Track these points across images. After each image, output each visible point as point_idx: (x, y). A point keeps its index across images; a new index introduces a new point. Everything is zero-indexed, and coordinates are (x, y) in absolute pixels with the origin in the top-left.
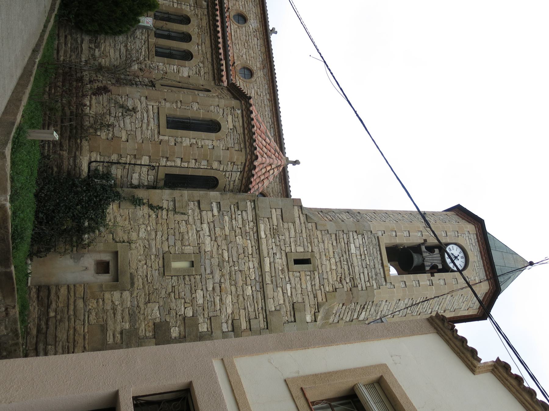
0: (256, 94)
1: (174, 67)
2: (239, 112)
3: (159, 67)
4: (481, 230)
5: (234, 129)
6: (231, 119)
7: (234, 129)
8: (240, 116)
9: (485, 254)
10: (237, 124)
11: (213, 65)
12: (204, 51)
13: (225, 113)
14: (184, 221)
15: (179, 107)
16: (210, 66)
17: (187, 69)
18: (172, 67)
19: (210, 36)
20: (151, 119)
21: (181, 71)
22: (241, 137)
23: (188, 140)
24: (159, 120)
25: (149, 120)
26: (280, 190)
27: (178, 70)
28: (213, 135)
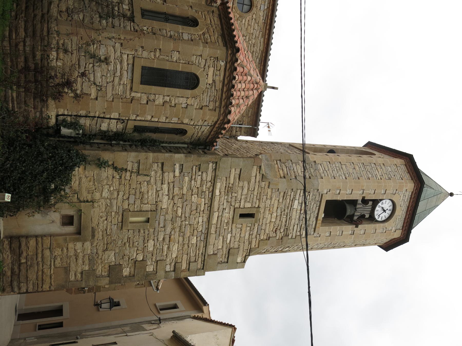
2: (223, 64)
6: (213, 72)
8: (223, 69)
10: (217, 78)
15: (157, 56)
20: (124, 72)
22: (218, 94)
23: (161, 97)
28: (189, 92)
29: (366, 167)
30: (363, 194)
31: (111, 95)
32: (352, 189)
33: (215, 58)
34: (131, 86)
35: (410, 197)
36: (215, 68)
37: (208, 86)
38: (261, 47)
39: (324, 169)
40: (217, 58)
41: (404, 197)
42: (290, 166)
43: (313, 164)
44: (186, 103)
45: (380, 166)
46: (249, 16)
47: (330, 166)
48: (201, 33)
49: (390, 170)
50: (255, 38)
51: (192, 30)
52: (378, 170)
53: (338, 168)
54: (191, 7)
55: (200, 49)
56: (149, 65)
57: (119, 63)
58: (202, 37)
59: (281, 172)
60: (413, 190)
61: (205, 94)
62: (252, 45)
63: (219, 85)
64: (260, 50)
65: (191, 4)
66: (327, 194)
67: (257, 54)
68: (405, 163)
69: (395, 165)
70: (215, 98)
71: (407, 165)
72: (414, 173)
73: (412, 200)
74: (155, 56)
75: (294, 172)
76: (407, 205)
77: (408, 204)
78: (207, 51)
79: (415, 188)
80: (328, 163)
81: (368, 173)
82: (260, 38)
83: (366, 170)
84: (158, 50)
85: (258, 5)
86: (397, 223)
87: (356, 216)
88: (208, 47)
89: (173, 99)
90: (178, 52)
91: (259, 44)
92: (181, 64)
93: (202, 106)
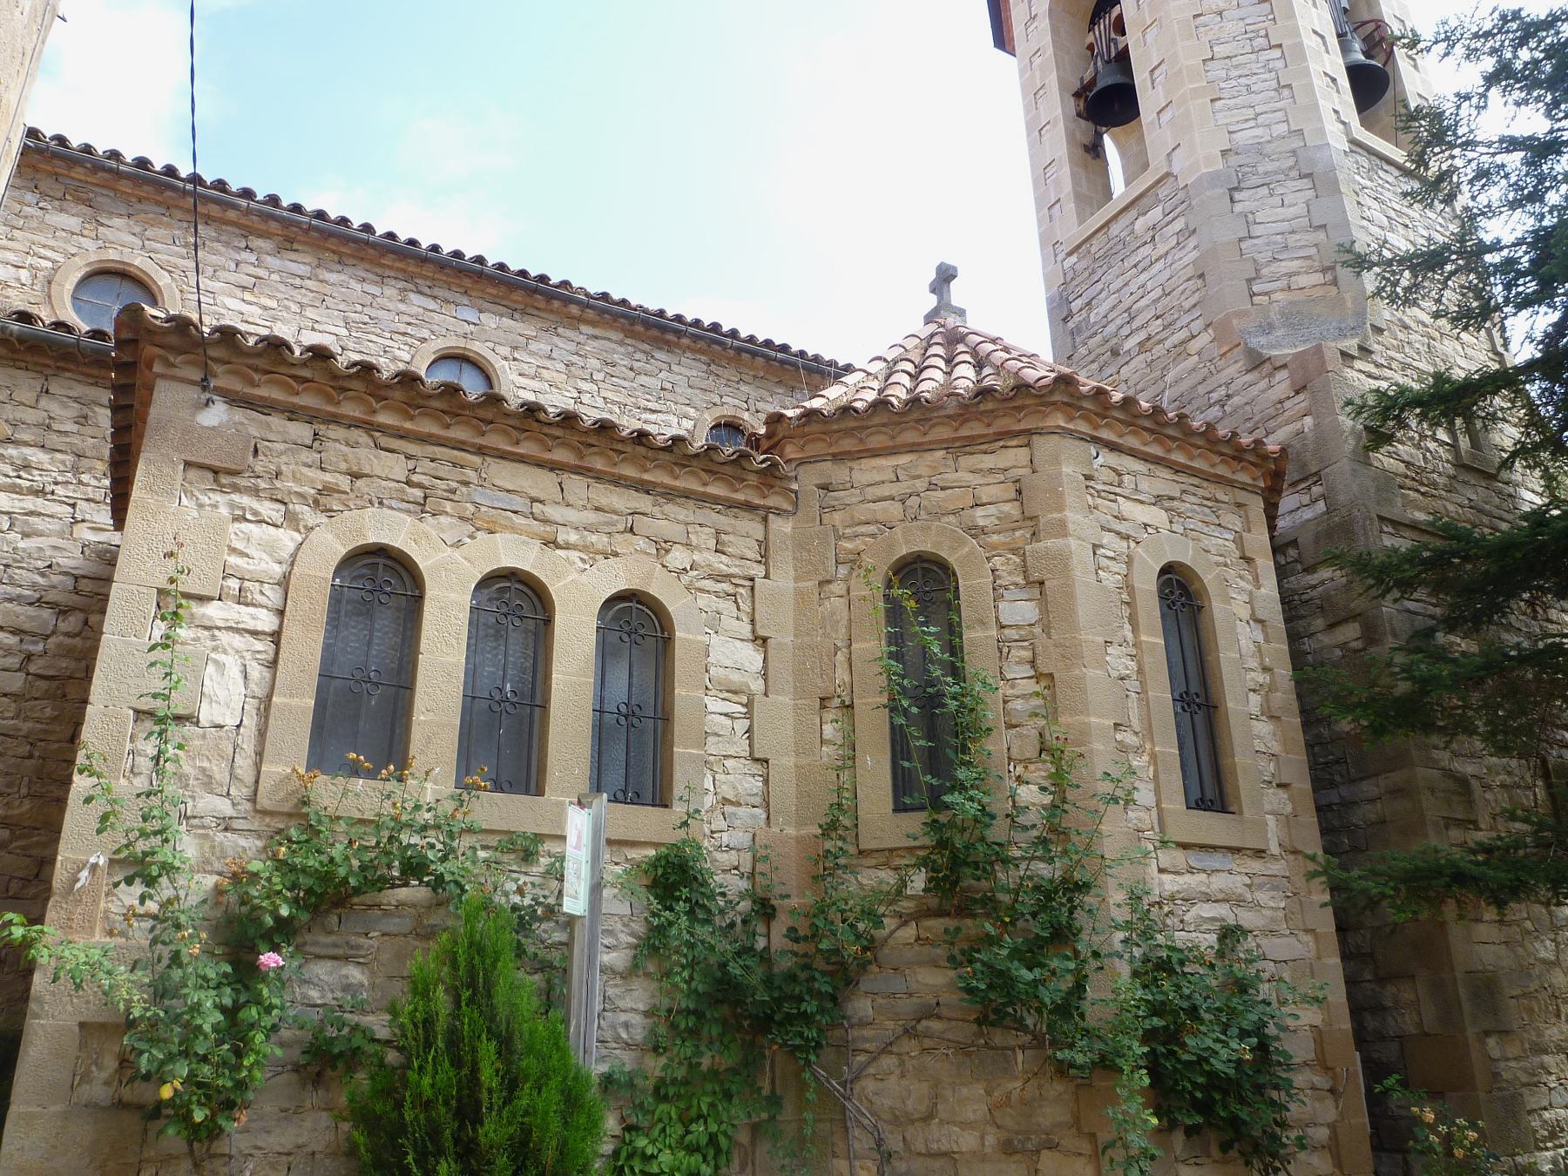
0: (247, 296)
11: (670, 494)
12: (591, 517)
16: (682, 512)
19: (481, 451)
20: (1214, 886)
21: (735, 677)
24: (1215, 848)
25: (1220, 896)
26: (699, 360)
27: (726, 695)
31: (1292, 940)
37: (1177, 528)
38: (614, 338)
39: (1252, 123)
42: (1268, 244)
43: (1234, 160)
46: (505, 372)
47: (1233, 101)
50: (581, 356)
51: (972, 585)
53: (1234, 73)
54: (823, 583)
59: (1303, 281)
62: (609, 369)
64: (621, 343)
65: (809, 584)
67: (638, 356)
75: (1293, 232)
80: (1219, 104)
85: (461, 331)
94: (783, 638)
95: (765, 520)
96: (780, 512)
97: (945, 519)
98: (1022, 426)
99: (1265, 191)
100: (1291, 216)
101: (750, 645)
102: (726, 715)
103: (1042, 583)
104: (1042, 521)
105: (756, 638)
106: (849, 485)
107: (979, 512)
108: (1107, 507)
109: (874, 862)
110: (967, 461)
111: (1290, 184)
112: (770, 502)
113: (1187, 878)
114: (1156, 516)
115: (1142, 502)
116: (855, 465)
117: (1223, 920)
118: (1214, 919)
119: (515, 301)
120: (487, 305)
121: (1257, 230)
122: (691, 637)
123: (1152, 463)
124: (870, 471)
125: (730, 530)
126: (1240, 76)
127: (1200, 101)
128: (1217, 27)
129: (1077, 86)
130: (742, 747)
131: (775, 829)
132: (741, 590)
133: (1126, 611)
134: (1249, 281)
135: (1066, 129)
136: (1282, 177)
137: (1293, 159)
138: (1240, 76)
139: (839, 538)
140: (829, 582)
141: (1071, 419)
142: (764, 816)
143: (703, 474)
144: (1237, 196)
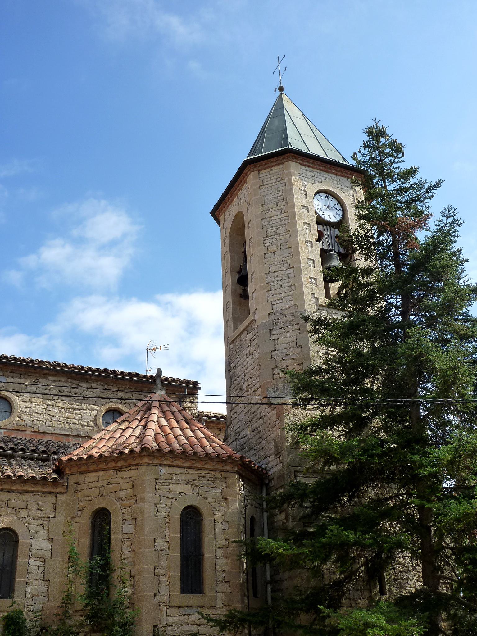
1: (31, 564)
2: (164, 470)
3: (36, 593)
4: (299, 156)
5: (191, 483)
6: (175, 485)
7: (191, 483)
8: (170, 470)
9: (324, 167)
10: (184, 478)
11: (21, 492)
13: (168, 495)
14: (331, 576)
15: (164, 571)
16: (24, 497)
17: (34, 541)
18: (32, 568)
21: (40, 553)
22: (205, 475)
23: (218, 561)
24: (192, 607)
26: (100, 384)
28: (207, 521)
29: (269, 234)
30: (311, 242)
32: (308, 258)
33: (156, 483)
34: (208, 607)
35: (307, 168)
36: (170, 481)
38: (63, 380)
39: (280, 301)
40: (156, 479)
41: (308, 176)
42: (281, 353)
43: (273, 317)
44: (222, 523)
45: (264, 211)
47: (275, 291)
48: (118, 503)
49: (271, 197)
50: (49, 390)
51: (116, 519)
52: (272, 215)
53: (276, 279)
55: (147, 507)
56: (178, 584)
57: (180, 629)
58: (125, 502)
60: (298, 163)
61: (207, 495)
63: (192, 474)
66: (317, 298)
68: (256, 171)
69: (261, 187)
70: (210, 479)
71: (260, 168)
72: (272, 160)
73: (312, 165)
74: (164, 575)
76: (318, 171)
77: (317, 170)
78: (149, 495)
79: (295, 160)
80: (270, 292)
81: (280, 232)
82: (49, 382)
83: (274, 234)
84: (156, 571)
86: (343, 187)
87: (339, 249)
88: (142, 495)
89: (219, 544)
90: (155, 540)
91: (58, 382)
92: (171, 535)
93: (223, 498)
94: (59, 537)
95: (56, 496)
96: (61, 493)
97: (111, 495)
98: (136, 462)
99: (282, 330)
100: (291, 341)
101: (47, 541)
102: (36, 566)
103: (136, 519)
104: (138, 496)
105: (49, 538)
106: (83, 483)
107: (121, 493)
108: (164, 489)
109: (80, 614)
110: (120, 474)
111: (291, 327)
112: (58, 490)
113: (179, 618)
114: (187, 488)
115: (181, 484)
116: (86, 475)
117: (193, 631)
118: (189, 631)
119: (22, 371)
120: (10, 374)
121: (278, 347)
122: (25, 541)
123: (187, 468)
124: (91, 477)
125: (43, 501)
126: (278, 280)
127: (263, 292)
128: (272, 258)
129: (238, 269)
130: (41, 576)
131: (50, 604)
132: (45, 522)
133: (167, 525)
134: (273, 369)
135: (232, 289)
136: (288, 324)
137: (293, 317)
138: (278, 280)
139: (79, 501)
140: (75, 517)
141: (150, 460)
142: (47, 599)
143: (32, 485)
144: (273, 332)
